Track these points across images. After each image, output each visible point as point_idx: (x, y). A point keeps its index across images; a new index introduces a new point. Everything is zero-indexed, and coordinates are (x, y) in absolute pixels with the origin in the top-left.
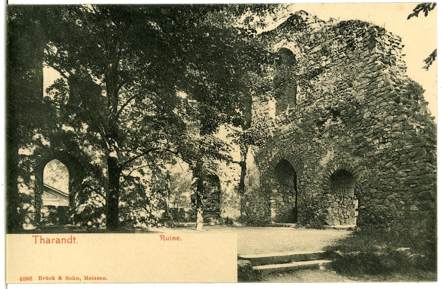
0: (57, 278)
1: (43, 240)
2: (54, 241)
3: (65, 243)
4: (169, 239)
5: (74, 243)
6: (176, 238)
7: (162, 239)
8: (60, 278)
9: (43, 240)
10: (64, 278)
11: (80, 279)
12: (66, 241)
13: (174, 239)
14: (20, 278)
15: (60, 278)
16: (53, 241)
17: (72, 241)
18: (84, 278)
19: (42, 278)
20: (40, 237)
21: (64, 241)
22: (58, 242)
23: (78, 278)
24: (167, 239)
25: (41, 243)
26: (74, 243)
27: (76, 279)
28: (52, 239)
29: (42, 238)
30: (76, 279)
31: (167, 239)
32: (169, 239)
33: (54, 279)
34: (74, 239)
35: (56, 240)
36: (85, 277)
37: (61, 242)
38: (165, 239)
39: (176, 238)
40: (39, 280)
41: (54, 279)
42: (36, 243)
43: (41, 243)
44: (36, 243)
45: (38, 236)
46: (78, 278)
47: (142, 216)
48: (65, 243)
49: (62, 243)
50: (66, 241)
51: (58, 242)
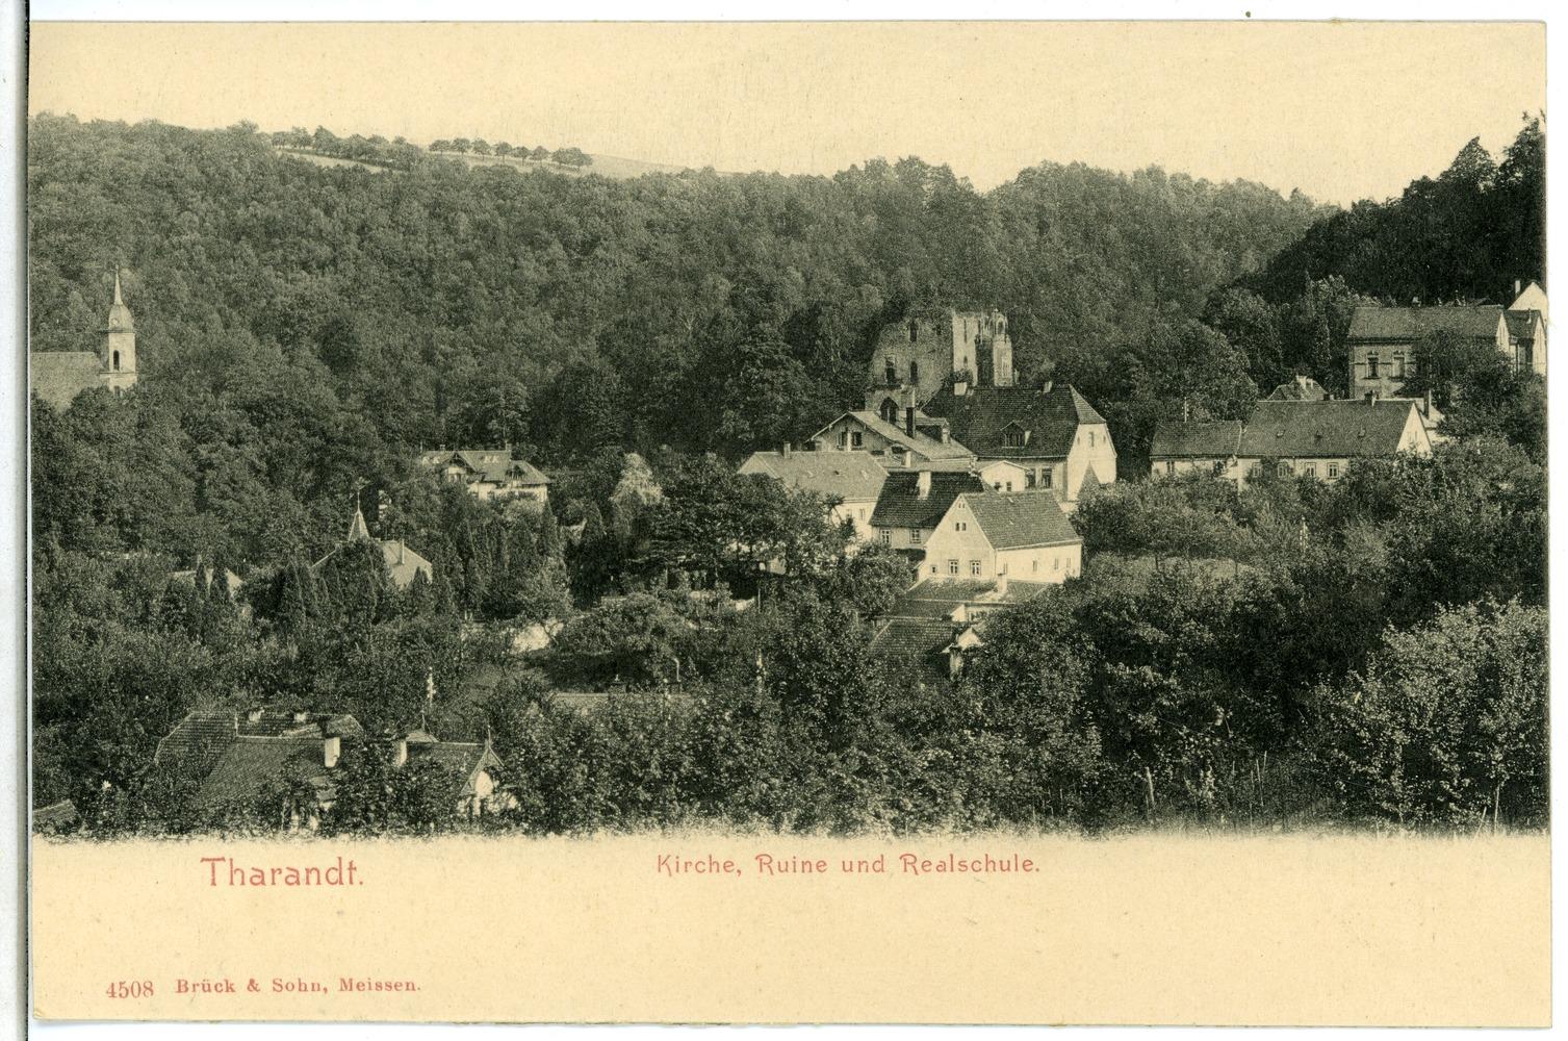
0: (241, 984)
1: (239, 874)
2: (279, 878)
3: (319, 883)
4: (791, 866)
5: (351, 882)
6: (814, 863)
7: (664, 868)
8: (252, 985)
9: (239, 874)
10: (265, 985)
11: (325, 990)
12: (870, 866)
13: (807, 867)
14: (109, 986)
15: (252, 985)
16: (277, 876)
17: (344, 874)
18: (338, 985)
19: (190, 986)
20: (228, 862)
21: (313, 877)
22: (291, 880)
23: (315, 987)
24: (783, 867)
25: (232, 883)
26: (351, 882)
27: (309, 987)
28: (273, 871)
29: (235, 866)
30: (309, 987)
31: (783, 867)
32: (791, 866)
33: (230, 988)
34: (351, 868)
35: (286, 873)
36: (343, 981)
37: (268, 879)
38: (775, 870)
39: (814, 863)
40: (179, 991)
41: (230, 988)
42: (214, 884)
43: (232, 883)
44: (214, 884)
45: (223, 859)
46: (315, 987)
47: (1499, 165)
48: (319, 883)
49: (308, 883)
50: (870, 866)
51: (291, 880)
